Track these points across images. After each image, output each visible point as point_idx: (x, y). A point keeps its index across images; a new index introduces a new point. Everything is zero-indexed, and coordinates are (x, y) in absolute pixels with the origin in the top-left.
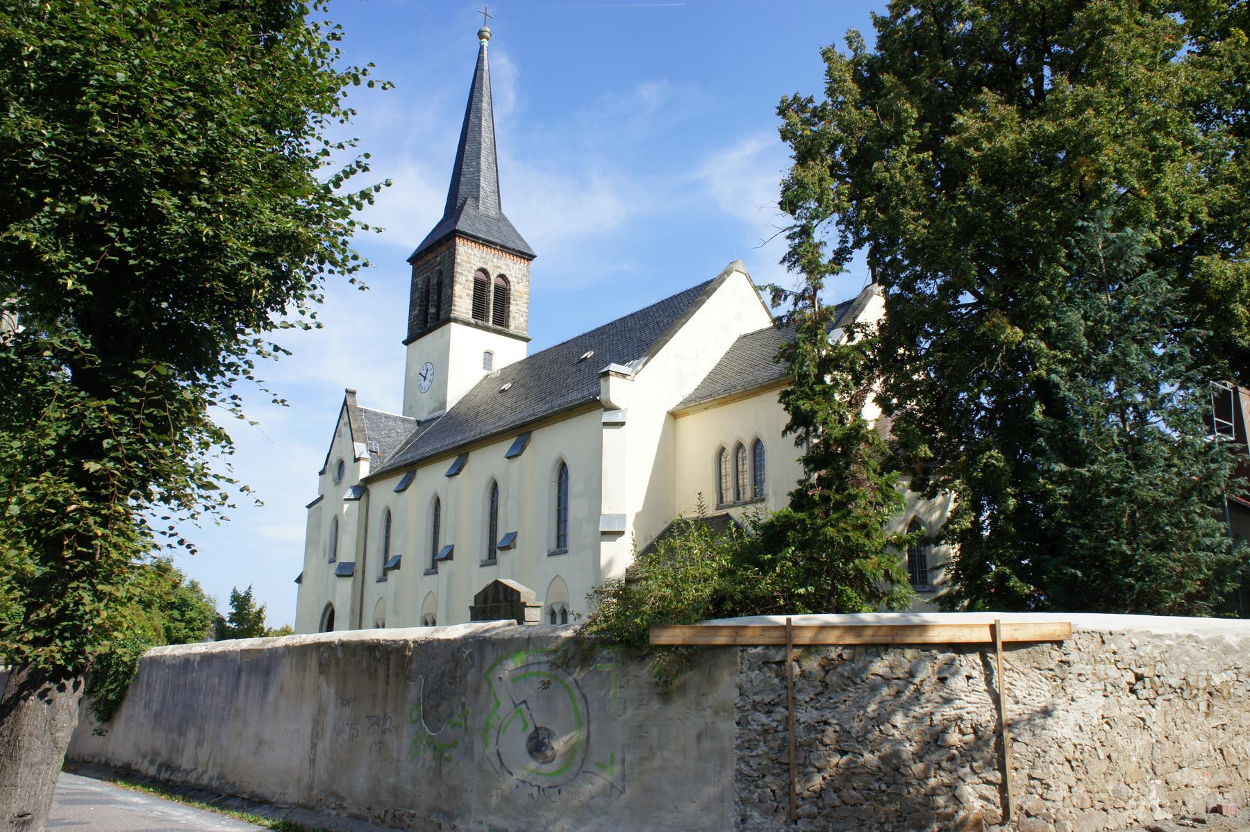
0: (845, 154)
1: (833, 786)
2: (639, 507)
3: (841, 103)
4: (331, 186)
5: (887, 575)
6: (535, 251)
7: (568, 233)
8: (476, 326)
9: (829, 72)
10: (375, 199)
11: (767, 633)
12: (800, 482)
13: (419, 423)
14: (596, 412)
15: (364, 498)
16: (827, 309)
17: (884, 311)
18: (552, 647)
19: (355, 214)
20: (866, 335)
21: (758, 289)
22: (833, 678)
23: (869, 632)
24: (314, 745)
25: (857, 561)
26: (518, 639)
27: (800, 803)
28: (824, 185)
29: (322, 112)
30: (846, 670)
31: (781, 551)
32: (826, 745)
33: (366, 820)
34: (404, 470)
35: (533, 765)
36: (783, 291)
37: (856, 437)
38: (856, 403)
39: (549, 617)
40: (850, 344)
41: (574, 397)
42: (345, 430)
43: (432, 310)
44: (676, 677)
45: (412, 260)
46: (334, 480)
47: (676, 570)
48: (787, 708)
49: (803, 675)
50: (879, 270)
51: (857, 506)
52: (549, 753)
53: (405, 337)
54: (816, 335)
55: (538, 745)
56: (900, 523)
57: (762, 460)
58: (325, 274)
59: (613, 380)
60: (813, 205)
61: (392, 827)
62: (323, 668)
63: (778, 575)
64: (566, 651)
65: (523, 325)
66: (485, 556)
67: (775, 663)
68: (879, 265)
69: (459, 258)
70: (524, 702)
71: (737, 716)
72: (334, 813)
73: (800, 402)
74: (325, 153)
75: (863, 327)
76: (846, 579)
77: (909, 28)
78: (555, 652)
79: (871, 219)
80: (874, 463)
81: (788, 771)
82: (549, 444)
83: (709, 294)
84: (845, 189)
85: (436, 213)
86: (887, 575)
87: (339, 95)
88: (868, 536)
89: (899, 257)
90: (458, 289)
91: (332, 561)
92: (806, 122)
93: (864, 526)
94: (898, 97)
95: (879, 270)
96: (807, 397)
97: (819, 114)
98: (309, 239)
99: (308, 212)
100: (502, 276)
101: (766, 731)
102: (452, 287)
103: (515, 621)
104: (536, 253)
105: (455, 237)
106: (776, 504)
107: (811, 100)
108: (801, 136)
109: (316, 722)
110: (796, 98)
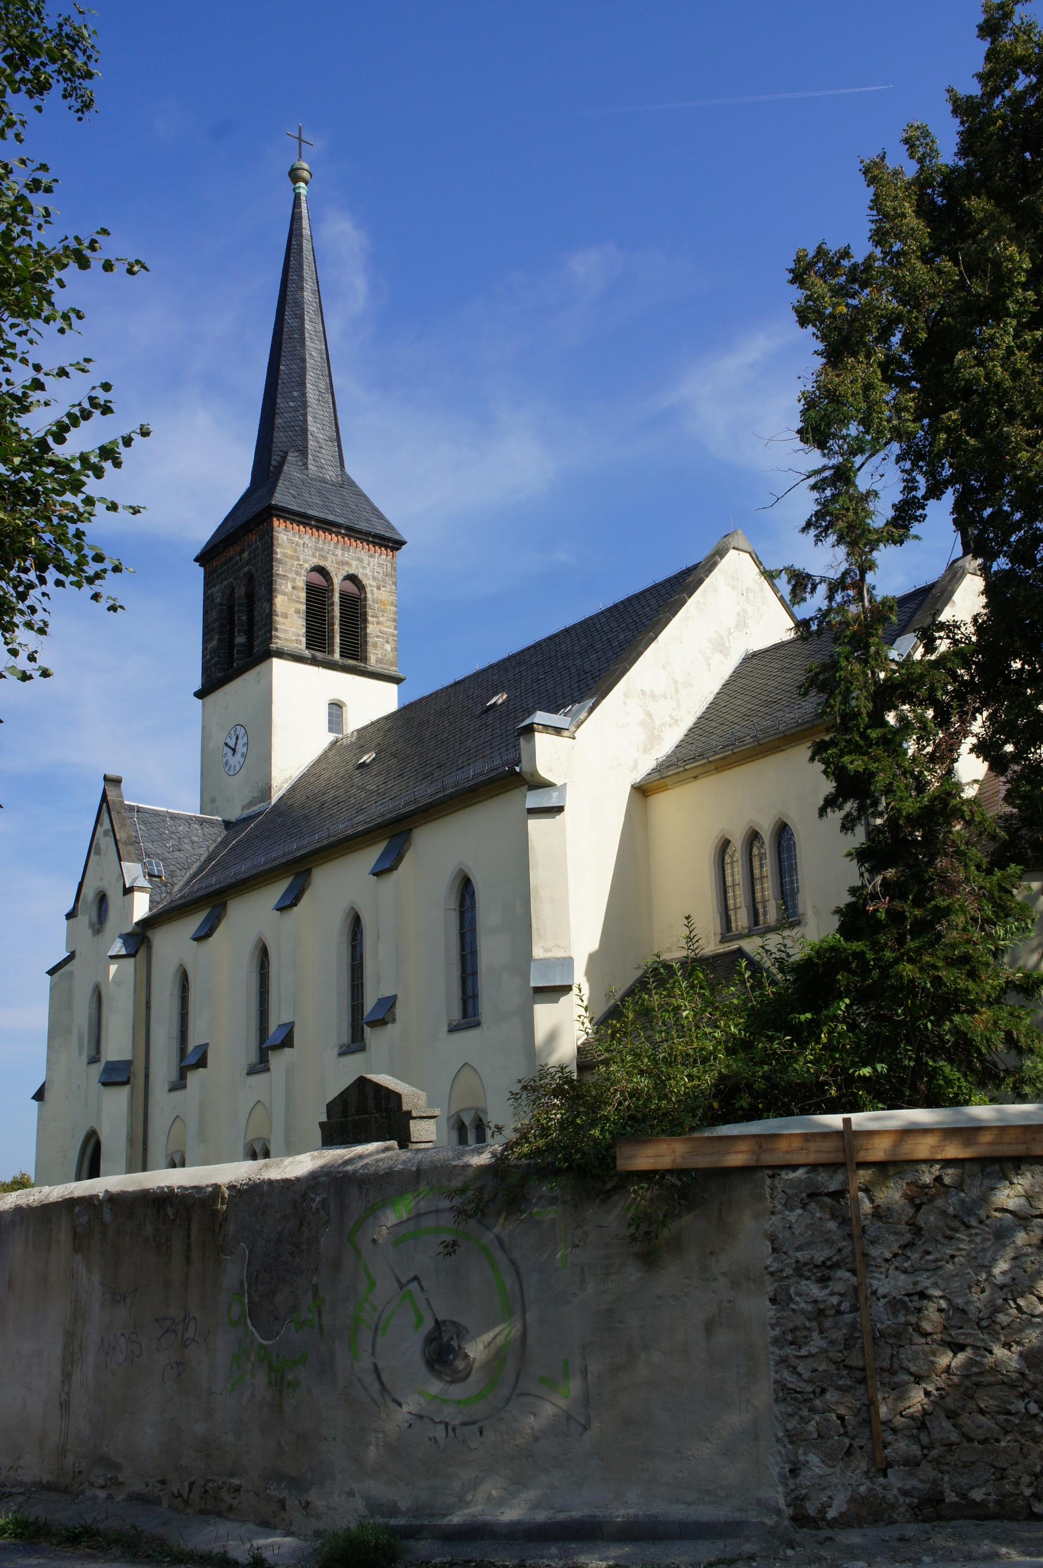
0: (906, 341)
1: (942, 1406)
2: (593, 943)
3: (898, 254)
4: (50, 440)
5: (1010, 1040)
6: (404, 534)
7: (456, 496)
8: (314, 662)
9: (876, 203)
10: (123, 458)
11: (812, 1146)
12: (853, 891)
13: (227, 824)
14: (515, 794)
15: (142, 954)
16: (883, 603)
17: (984, 600)
18: (457, 1183)
19: (92, 486)
20: (955, 642)
21: (770, 576)
22: (929, 1219)
23: (986, 1138)
24: (67, 1377)
25: (956, 1018)
26: (400, 1172)
27: (889, 1437)
28: (874, 395)
29: (26, 317)
30: (951, 1204)
31: (827, 1007)
32: (926, 1335)
33: (158, 1502)
34: (204, 902)
35: (435, 1387)
36: (809, 576)
37: (942, 812)
38: (946, 755)
39: (455, 1135)
40: (929, 657)
41: (477, 769)
42: (106, 843)
43: (240, 639)
44: (664, 1224)
45: (203, 559)
46: (92, 925)
47: (655, 1045)
48: (854, 1272)
49: (877, 1213)
50: (973, 531)
51: (951, 927)
52: (460, 1364)
53: (197, 685)
54: (867, 646)
55: (441, 1353)
56: (1033, 951)
57: (792, 857)
58: (50, 587)
59: (542, 741)
60: (854, 429)
61: (201, 1512)
62: (79, 1242)
63: (825, 1047)
64: (481, 1190)
65: (391, 656)
66: (346, 1038)
67: (828, 1195)
68: (972, 522)
69: (279, 552)
70: (416, 1278)
71: (770, 1287)
72: (102, 1494)
73: (846, 759)
74: (38, 385)
75: (950, 628)
76: (938, 1050)
77: (1015, 112)
78: (462, 1191)
79: (955, 447)
80: (976, 853)
81: (863, 1381)
82: (441, 849)
83: (691, 590)
84: (909, 400)
85: (240, 480)
86: (1010, 1040)
87: (52, 285)
88: (973, 975)
89: (1006, 508)
90: (280, 602)
91: (94, 1060)
92: (840, 292)
93: (965, 959)
94: (995, 236)
95: (973, 531)
96: (858, 750)
97: (862, 275)
98: (18, 530)
99: (12, 484)
100: (352, 578)
101: (821, 1312)
102: (270, 600)
103: (394, 1143)
104: (405, 537)
105: (271, 516)
106: (817, 929)
107: (846, 254)
108: (832, 316)
109: (70, 1336)
110: (821, 252)
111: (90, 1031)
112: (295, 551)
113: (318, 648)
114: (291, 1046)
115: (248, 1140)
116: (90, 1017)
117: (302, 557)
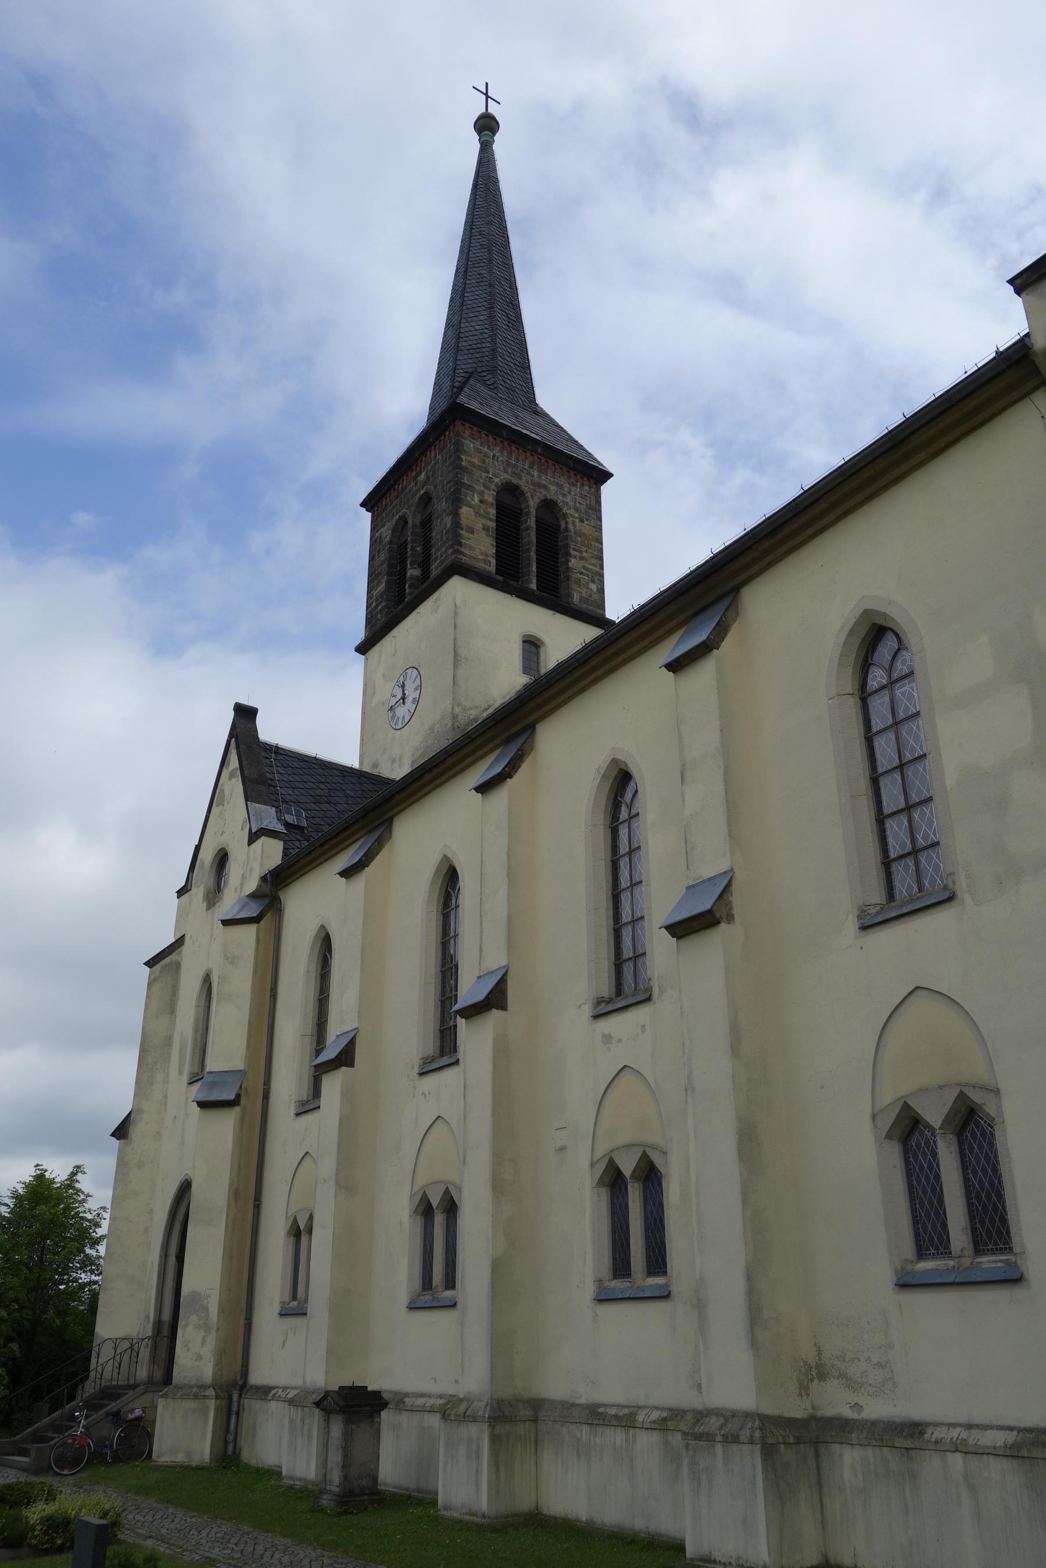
43: (413, 572)
53: (359, 633)
111: (195, 1040)
112: (484, 462)
113: (506, 578)
114: (503, 1007)
115: (418, 1186)
116: (197, 1020)
117: (491, 470)
